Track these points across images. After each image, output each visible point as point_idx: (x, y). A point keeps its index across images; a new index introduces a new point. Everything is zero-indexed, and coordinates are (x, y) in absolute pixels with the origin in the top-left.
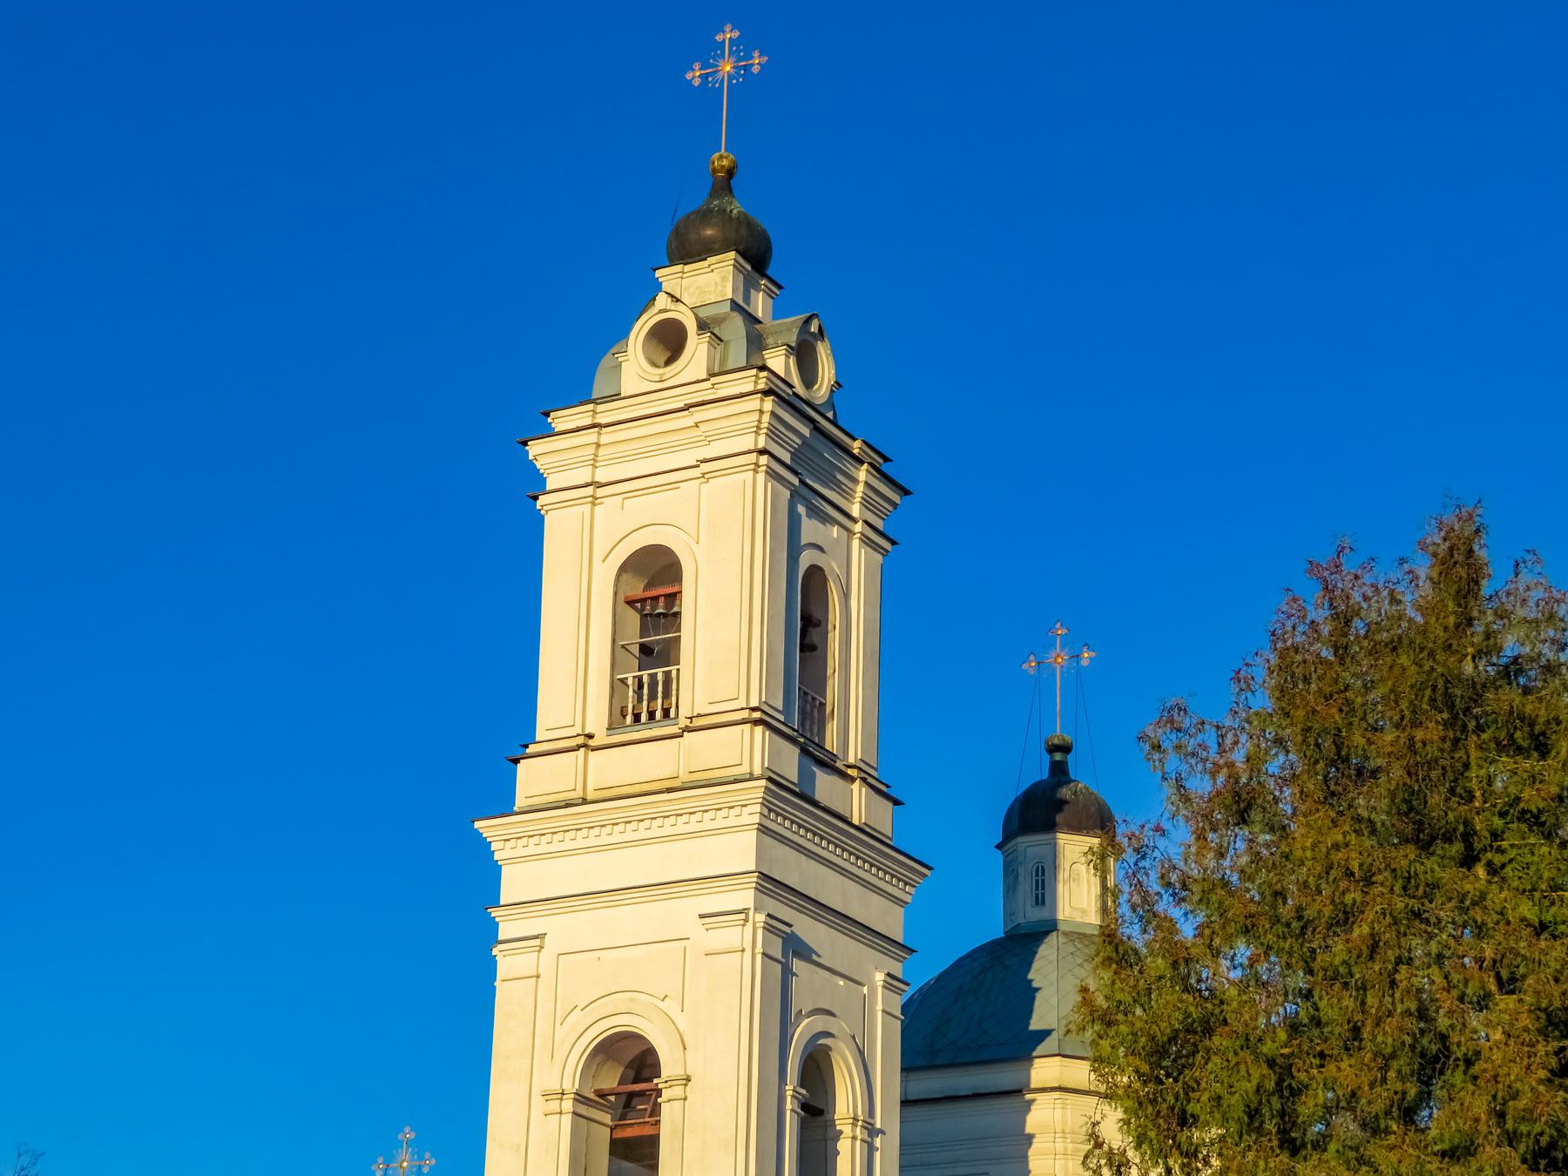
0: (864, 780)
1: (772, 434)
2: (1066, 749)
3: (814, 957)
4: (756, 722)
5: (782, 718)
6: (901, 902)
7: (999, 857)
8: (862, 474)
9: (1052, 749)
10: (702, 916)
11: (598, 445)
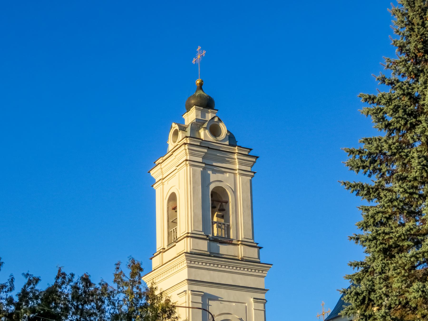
0: (241, 244)
1: (191, 154)
3: (220, 299)
5: (203, 233)
6: (263, 277)
8: (236, 156)
10: (178, 295)
11: (161, 169)
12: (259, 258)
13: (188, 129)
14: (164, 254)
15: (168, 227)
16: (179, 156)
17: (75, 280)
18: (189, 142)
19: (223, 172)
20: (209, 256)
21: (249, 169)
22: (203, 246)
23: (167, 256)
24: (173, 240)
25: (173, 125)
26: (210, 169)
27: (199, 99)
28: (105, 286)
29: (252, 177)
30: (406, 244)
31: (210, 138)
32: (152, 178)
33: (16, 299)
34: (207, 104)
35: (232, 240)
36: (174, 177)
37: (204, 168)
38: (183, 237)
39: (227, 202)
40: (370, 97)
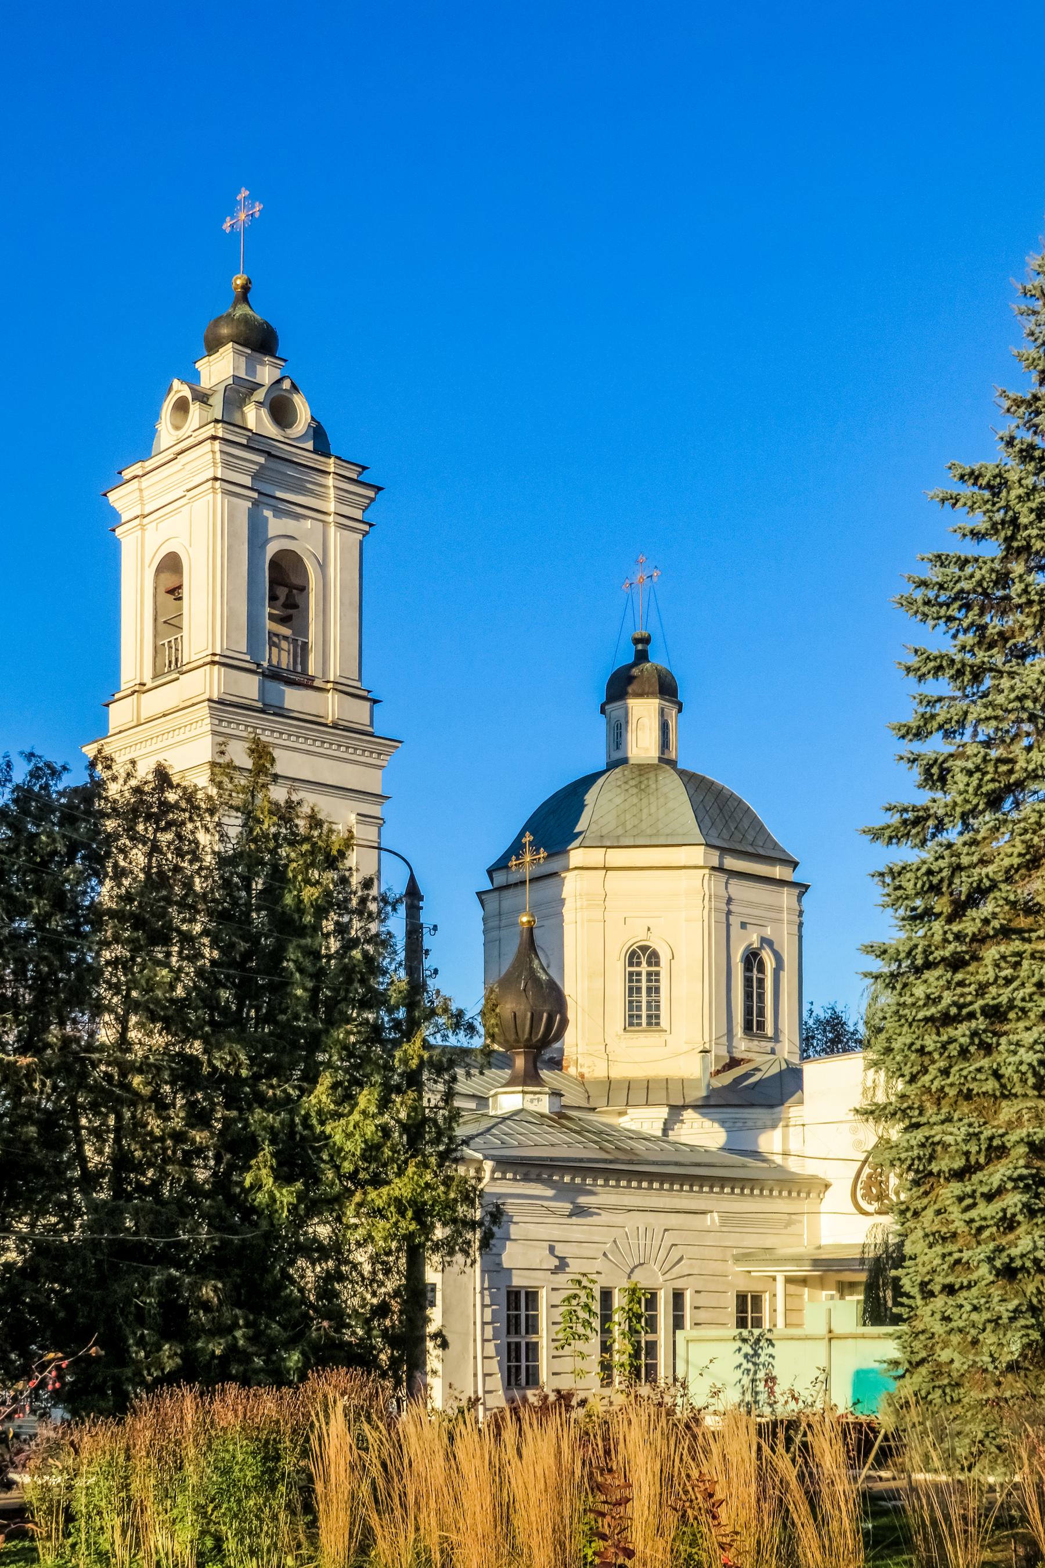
1: (226, 465)
2: (646, 641)
4: (213, 663)
5: (248, 658)
7: (603, 719)
8: (330, 481)
9: (637, 641)
12: (371, 725)
13: (217, 401)
14: (143, 696)
15: (156, 636)
16: (194, 464)
18: (220, 435)
19: (298, 517)
20: (262, 711)
21: (358, 514)
22: (249, 687)
23: (154, 702)
24: (169, 664)
25: (176, 383)
26: (269, 506)
27: (242, 328)
29: (366, 534)
31: (271, 429)
32: (113, 508)
34: (260, 341)
35: (313, 678)
37: (256, 503)
38: (201, 662)
39: (303, 589)
40: (972, 473)
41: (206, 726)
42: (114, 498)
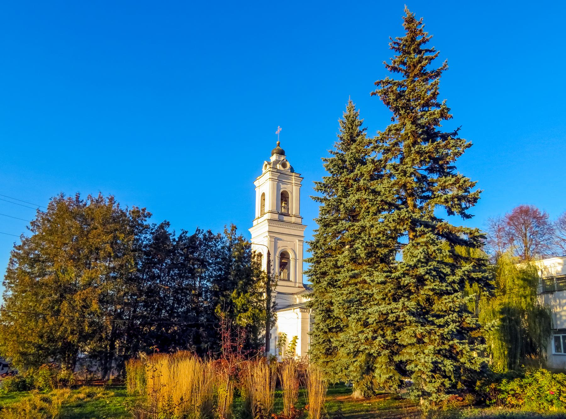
1: (272, 176)
13: (272, 164)
17: (204, 232)
19: (287, 184)
22: (276, 216)
23: (260, 220)
24: (263, 214)
28: (219, 235)
30: (333, 223)
31: (282, 168)
33: (177, 240)
34: (282, 153)
36: (264, 185)
39: (288, 198)
41: (267, 224)
42: (256, 183)
